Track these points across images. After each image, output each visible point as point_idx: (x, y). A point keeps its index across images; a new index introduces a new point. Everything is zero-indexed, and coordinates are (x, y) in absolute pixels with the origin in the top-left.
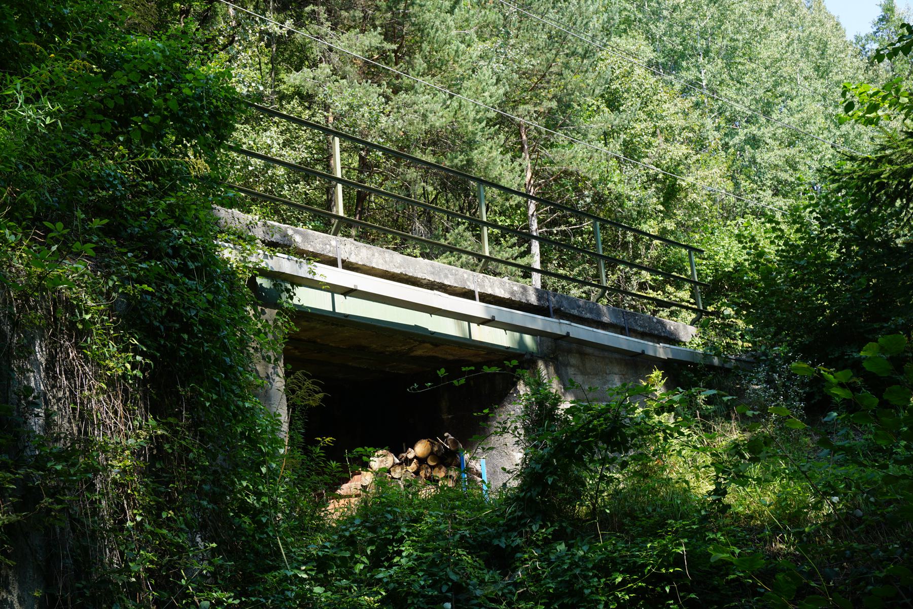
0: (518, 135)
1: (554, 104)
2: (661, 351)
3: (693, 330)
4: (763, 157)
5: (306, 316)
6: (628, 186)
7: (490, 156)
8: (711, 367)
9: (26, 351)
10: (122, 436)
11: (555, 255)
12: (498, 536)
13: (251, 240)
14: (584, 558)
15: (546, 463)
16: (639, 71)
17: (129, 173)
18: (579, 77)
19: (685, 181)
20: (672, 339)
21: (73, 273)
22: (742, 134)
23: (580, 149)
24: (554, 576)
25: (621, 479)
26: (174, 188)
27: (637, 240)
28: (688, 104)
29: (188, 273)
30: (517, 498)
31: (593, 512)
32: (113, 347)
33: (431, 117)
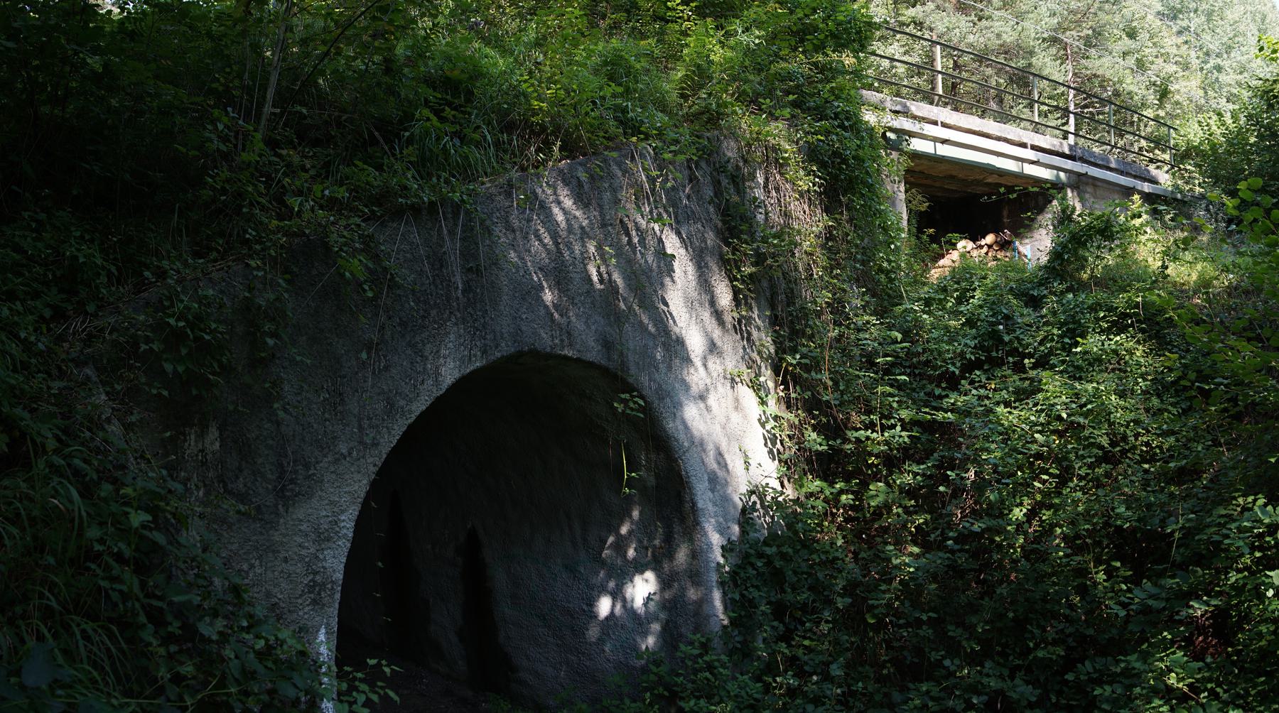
0: (1065, 49)
1: (1090, 32)
2: (1147, 187)
3: (1167, 176)
4: (1223, 78)
5: (916, 156)
6: (1135, 86)
7: (1045, 62)
8: (1176, 199)
9: (752, 177)
10: (809, 223)
11: (1085, 127)
12: (1033, 289)
13: (884, 109)
14: (1083, 303)
15: (1064, 246)
16: (1150, 17)
17: (806, 69)
18: (1110, 17)
19: (1173, 87)
20: (1153, 181)
21: (777, 132)
22: (1212, 62)
23: (1106, 61)
24: (1064, 312)
25: (1110, 260)
26: (833, 78)
27: (1140, 120)
28: (1180, 40)
29: (844, 128)
30: (1046, 267)
31: (1092, 277)
32: (802, 173)
33: (1005, 36)
